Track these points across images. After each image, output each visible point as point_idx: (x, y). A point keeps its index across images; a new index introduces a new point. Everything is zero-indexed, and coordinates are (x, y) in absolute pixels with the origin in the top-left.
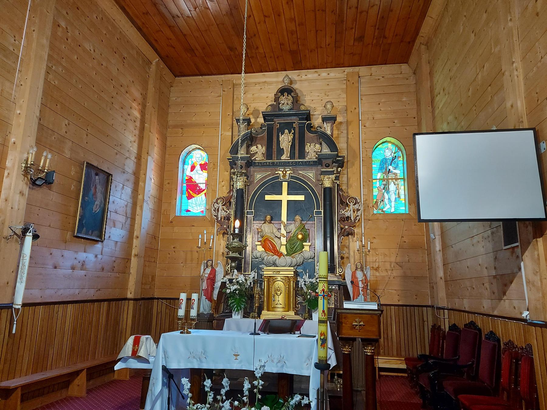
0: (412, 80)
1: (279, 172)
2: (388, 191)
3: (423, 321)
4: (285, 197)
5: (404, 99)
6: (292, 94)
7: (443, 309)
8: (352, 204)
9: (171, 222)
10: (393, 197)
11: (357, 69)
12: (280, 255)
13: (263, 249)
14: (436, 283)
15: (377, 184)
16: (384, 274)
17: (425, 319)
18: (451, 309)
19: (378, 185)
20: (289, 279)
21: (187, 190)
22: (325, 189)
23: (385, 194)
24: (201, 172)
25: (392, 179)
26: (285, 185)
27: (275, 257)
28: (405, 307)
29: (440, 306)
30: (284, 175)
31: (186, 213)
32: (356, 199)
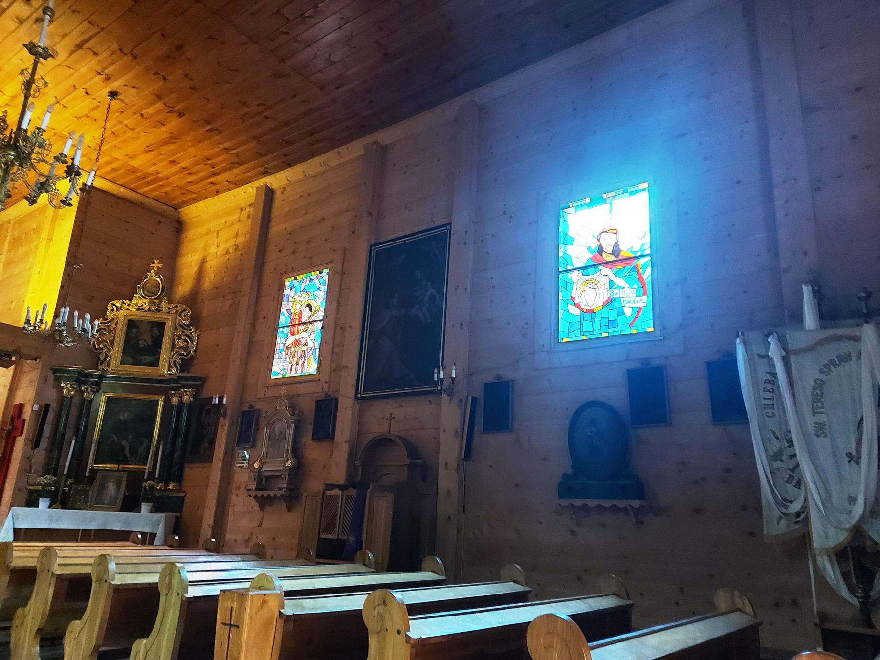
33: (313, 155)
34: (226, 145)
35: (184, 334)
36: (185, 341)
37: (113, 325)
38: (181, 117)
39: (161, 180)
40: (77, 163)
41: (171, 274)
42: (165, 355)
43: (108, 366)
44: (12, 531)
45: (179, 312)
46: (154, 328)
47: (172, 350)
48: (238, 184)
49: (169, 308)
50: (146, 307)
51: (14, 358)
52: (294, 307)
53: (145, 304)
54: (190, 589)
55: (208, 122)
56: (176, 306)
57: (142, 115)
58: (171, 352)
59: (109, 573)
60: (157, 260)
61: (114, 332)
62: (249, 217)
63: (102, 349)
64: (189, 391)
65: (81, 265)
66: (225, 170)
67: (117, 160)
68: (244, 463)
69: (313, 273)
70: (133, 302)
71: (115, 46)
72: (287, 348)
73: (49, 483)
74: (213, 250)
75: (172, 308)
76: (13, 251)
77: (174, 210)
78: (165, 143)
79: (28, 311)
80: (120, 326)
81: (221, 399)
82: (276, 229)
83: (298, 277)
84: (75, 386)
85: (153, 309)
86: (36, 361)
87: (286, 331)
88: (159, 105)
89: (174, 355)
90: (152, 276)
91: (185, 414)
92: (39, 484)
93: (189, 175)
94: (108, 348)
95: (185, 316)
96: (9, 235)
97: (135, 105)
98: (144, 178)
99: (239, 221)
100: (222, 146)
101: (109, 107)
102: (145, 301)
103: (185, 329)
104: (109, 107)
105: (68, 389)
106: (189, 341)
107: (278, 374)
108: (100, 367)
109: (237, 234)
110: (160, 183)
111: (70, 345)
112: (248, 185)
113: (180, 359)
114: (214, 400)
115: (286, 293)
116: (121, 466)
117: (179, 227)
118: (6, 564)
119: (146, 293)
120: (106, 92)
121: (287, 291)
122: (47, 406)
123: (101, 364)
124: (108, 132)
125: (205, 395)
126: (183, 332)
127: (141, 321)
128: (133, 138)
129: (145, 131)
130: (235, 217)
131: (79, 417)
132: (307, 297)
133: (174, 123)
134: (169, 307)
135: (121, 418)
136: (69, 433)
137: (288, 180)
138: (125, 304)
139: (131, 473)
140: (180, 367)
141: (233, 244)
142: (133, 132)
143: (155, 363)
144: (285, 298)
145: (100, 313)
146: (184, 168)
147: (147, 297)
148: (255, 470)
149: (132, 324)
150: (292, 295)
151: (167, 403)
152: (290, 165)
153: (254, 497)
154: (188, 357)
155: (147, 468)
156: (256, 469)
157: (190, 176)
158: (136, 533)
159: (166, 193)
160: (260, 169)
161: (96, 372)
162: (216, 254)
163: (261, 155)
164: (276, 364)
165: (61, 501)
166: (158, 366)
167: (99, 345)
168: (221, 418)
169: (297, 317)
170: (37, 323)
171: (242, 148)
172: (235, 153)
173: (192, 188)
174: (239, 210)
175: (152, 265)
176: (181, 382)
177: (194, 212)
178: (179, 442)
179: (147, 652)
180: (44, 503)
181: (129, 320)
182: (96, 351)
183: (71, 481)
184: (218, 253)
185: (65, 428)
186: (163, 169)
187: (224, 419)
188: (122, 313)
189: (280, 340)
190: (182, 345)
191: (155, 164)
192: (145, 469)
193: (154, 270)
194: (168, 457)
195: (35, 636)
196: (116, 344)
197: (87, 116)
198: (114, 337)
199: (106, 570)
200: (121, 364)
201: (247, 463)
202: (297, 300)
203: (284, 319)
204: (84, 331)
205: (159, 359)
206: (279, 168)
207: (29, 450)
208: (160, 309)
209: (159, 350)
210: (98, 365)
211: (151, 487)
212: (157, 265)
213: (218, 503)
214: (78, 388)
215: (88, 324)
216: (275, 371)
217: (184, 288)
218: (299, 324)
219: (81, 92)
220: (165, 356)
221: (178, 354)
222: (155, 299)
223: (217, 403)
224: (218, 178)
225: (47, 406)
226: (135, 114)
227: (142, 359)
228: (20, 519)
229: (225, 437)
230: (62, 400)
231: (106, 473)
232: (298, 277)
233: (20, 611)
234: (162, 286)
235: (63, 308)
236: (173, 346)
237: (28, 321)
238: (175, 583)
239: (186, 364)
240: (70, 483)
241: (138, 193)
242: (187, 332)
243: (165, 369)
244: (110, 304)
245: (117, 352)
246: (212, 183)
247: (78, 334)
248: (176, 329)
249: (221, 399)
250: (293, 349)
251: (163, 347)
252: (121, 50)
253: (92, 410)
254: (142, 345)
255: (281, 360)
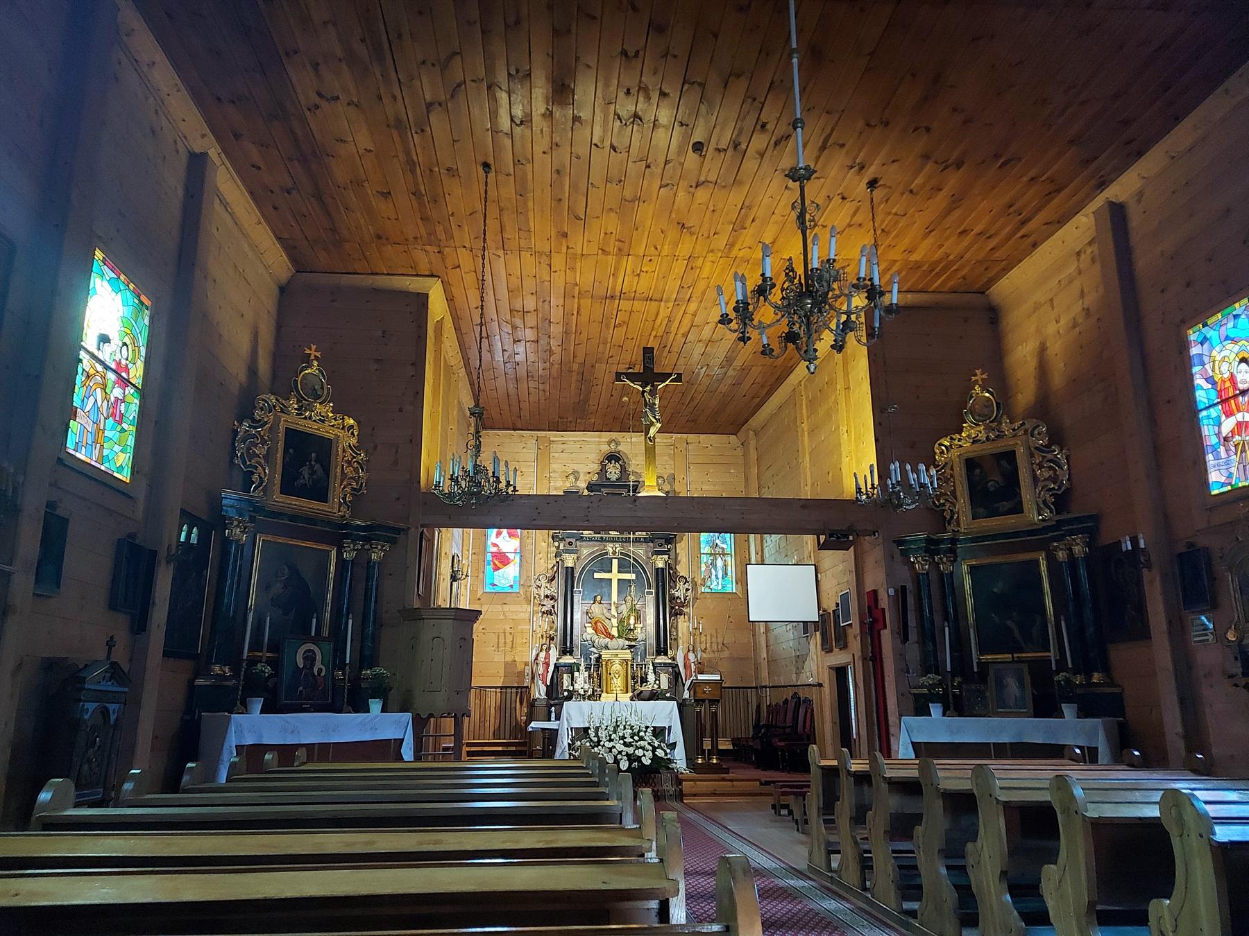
0: (740, 452)
1: (608, 548)
2: (715, 566)
3: (748, 703)
4: (615, 576)
5: (732, 471)
6: (620, 462)
7: (766, 687)
8: (681, 583)
9: (479, 599)
10: (720, 575)
11: (685, 436)
12: (612, 637)
13: (594, 632)
14: (587, 518)
15: (704, 559)
16: (712, 655)
17: (750, 701)
18: (773, 687)
19: (705, 560)
20: (627, 663)
21: (493, 561)
22: (657, 569)
23: (713, 570)
24: (509, 539)
25: (720, 554)
26: (615, 562)
27: (608, 640)
28: (730, 690)
29: (763, 684)
30: (614, 553)
31: (491, 587)
32: (685, 578)
33: (1177, 119)
34: (1032, 173)
35: (1045, 460)
36: (1051, 468)
37: (949, 471)
38: (960, 168)
39: (953, 262)
40: (876, 282)
41: (1001, 382)
42: (1027, 495)
43: (958, 525)
44: (911, 745)
45: (1029, 431)
46: (1002, 462)
47: (1035, 487)
48: (1061, 221)
49: (1014, 430)
50: (982, 436)
51: (851, 538)
52: (1217, 371)
53: (981, 432)
54: (1217, 829)
55: (997, 156)
56: (1023, 424)
57: (911, 191)
58: (1035, 488)
59: (1078, 801)
60: (978, 369)
61: (952, 480)
62: (1093, 260)
63: (944, 505)
64: (1078, 538)
65: (895, 406)
66: (1038, 209)
67: (896, 261)
68: (1206, 635)
69: (1237, 305)
70: (963, 434)
71: (860, 124)
72: (1226, 439)
73: (935, 684)
74: (1051, 329)
75: (1018, 428)
76: (812, 416)
77: (979, 295)
78: (949, 211)
79: (856, 478)
80: (957, 469)
81: (1135, 541)
82: (1144, 260)
83: (1209, 322)
84: (927, 558)
85: (993, 437)
86: (875, 535)
87: (1214, 412)
88: (929, 167)
89: (1040, 493)
90: (978, 393)
91: (1083, 572)
92: (922, 686)
93: (989, 240)
94: (951, 503)
95: (1039, 434)
96: (804, 398)
97: (899, 183)
98: (932, 270)
99: (1080, 273)
100: (1025, 179)
101: (872, 202)
102: (978, 428)
103: (1043, 451)
104: (872, 202)
105: (920, 564)
106: (1057, 468)
107: (1223, 485)
108: (948, 528)
109: (1082, 292)
110: (954, 268)
111: (911, 507)
112: (1078, 214)
113: (1051, 496)
114: (1123, 545)
115: (1194, 353)
116: (1015, 655)
117: (993, 315)
118: (934, 786)
119: (977, 418)
120: (863, 185)
121: (1194, 351)
122: (904, 588)
123: (949, 524)
124: (879, 232)
125: (1106, 539)
126: (1044, 457)
127: (981, 457)
128: (907, 225)
129: (920, 209)
130: (1071, 269)
131: (944, 598)
132: (1236, 349)
133: (953, 181)
134: (1013, 427)
135: (995, 590)
136: (938, 618)
137: (1144, 178)
138: (955, 440)
139: (1030, 662)
140: (1055, 507)
141: (1081, 309)
142: (905, 218)
143: (1018, 509)
144: (1196, 361)
145: (931, 462)
146: (979, 234)
147: (980, 423)
148: (1231, 644)
149: (971, 464)
150: (1206, 353)
151: (1051, 559)
152: (1140, 154)
153: (1244, 687)
154: (1062, 491)
155: (1052, 654)
156: (1232, 641)
157: (991, 239)
158: (1071, 747)
159: (964, 278)
160: (1093, 182)
161: (946, 536)
162: (1059, 332)
163: (1088, 162)
164: (1212, 470)
165: (956, 707)
166: (1023, 512)
167: (938, 501)
168: (1145, 571)
169: (1228, 384)
170: (869, 490)
171: (1055, 167)
172: (1048, 178)
173: (997, 255)
174: (1075, 258)
175: (974, 378)
176: (1063, 528)
177: (1009, 286)
178: (1088, 614)
179: (1176, 920)
180: (936, 710)
181: (966, 459)
182: (938, 509)
183: (957, 680)
184: (1061, 332)
185: (931, 612)
186: (953, 247)
187: (1150, 571)
188: (955, 453)
189: (1208, 430)
190: (1048, 476)
191: (941, 246)
192: (1050, 656)
193: (979, 385)
194: (1078, 635)
195: (1000, 881)
196: (958, 494)
197: (850, 225)
198: (954, 486)
199: (1072, 797)
200: (973, 519)
201: (1211, 633)
202: (1218, 358)
203: (1203, 394)
204: (923, 487)
205: (1021, 502)
206: (1121, 169)
207: (900, 645)
208: (1003, 434)
209: (1018, 490)
210: (945, 525)
211: (1067, 680)
212: (980, 376)
213: (1182, 701)
214: (931, 560)
215: (926, 476)
216: (1214, 480)
217: (1025, 395)
218: (1235, 396)
219: (837, 200)
220: (1028, 497)
221: (1046, 489)
222: (990, 422)
223: (1130, 548)
224: (1032, 225)
225: (904, 588)
226: (903, 194)
227: (999, 507)
228: (915, 731)
229: (1160, 598)
230: (917, 577)
231: (1001, 666)
232: (1209, 322)
233: (970, 846)
234: (996, 403)
235: (892, 464)
236: (1035, 480)
237: (859, 490)
238: (1188, 817)
239: (1061, 501)
240: (959, 682)
241: (930, 292)
242: (1050, 456)
243: (1034, 513)
244: (937, 445)
245: (963, 504)
246: (1023, 237)
247: (917, 492)
248: (1032, 455)
249: (1135, 541)
250: (1237, 438)
251: (1022, 484)
252: (868, 125)
253: (955, 585)
254: (992, 489)
255: (1221, 461)
